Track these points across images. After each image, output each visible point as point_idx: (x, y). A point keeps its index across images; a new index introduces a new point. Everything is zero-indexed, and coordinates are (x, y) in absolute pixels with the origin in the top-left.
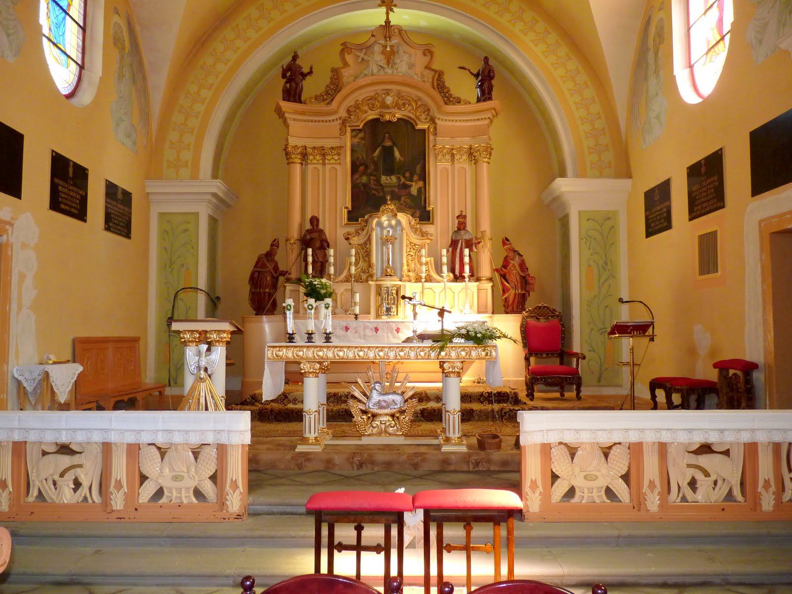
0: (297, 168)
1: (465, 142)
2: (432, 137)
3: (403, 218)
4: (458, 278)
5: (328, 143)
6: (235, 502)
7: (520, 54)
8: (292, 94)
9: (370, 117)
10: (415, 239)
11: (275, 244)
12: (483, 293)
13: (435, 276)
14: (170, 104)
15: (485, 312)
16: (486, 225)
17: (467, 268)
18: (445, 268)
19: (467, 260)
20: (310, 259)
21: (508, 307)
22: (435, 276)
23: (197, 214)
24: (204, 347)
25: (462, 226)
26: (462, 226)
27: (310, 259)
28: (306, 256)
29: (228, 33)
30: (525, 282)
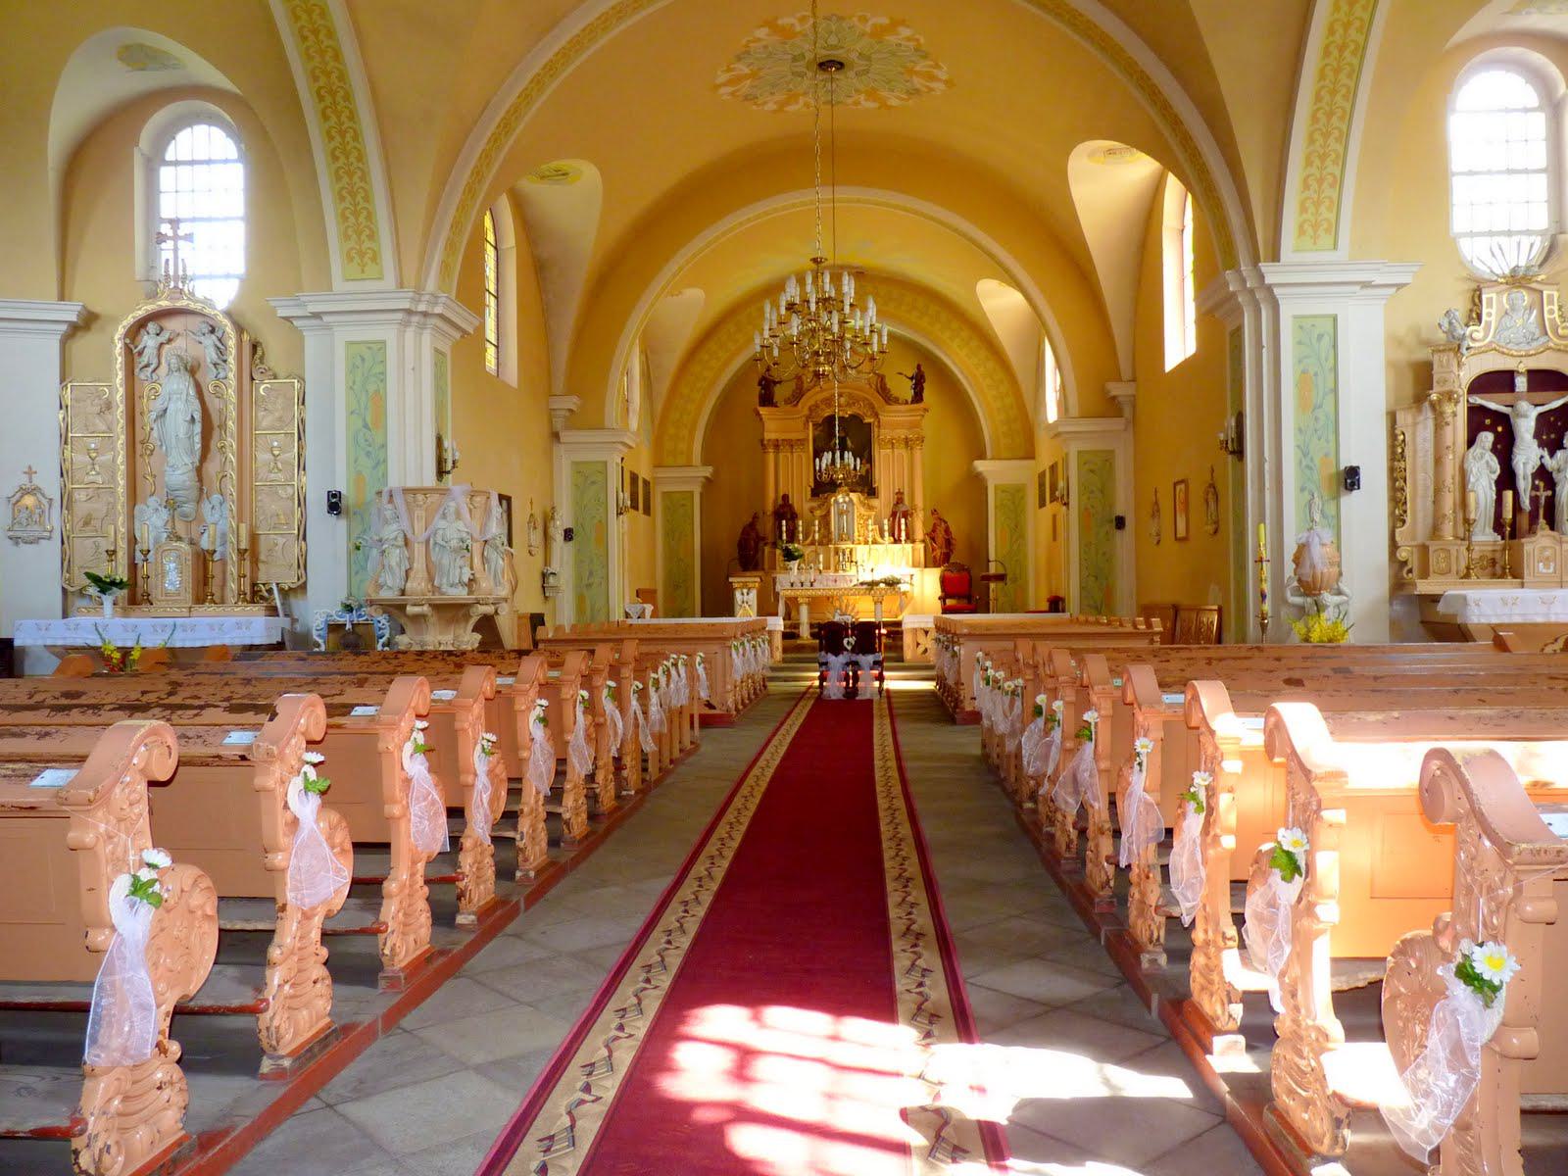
0: (771, 457)
1: (902, 433)
2: (876, 429)
3: (854, 496)
4: (897, 541)
5: (793, 436)
6: (779, 655)
7: (946, 355)
8: (767, 400)
9: (826, 415)
10: (863, 511)
11: (755, 517)
12: (916, 553)
13: (879, 539)
14: (667, 408)
15: (919, 566)
16: (919, 502)
17: (903, 534)
18: (886, 534)
19: (903, 527)
20: (784, 528)
21: (930, 562)
22: (879, 539)
23: (692, 493)
24: (745, 591)
25: (899, 501)
26: (899, 501)
27: (784, 528)
28: (781, 526)
29: (712, 345)
30: (949, 543)
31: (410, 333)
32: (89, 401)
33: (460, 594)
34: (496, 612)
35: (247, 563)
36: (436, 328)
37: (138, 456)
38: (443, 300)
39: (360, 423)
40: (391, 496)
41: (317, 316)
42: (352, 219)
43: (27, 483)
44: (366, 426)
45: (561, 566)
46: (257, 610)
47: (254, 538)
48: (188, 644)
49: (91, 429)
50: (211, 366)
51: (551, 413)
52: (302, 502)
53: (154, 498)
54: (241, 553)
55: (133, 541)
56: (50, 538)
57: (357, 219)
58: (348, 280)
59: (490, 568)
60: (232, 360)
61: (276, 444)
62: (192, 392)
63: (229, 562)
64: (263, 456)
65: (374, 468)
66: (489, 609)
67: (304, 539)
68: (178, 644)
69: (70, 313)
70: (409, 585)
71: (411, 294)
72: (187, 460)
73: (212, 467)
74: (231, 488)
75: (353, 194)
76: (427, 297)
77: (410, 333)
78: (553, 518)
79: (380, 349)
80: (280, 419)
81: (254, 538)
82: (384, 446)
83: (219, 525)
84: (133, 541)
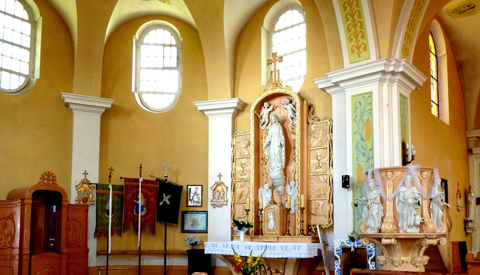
31: (385, 86)
32: (242, 142)
33: (414, 232)
34: (439, 243)
35: (305, 215)
36: (400, 81)
37: (260, 165)
38: (403, 63)
39: (359, 138)
40: (373, 174)
41: (336, 84)
42: (353, 30)
43: (218, 180)
44: (362, 139)
45: (475, 217)
46: (308, 239)
47: (308, 202)
48: (272, 256)
49: (243, 155)
50: (290, 119)
51: (467, 139)
52: (331, 183)
53: (266, 185)
54: (302, 209)
55: (257, 204)
56: (226, 205)
57: (355, 29)
58: (352, 63)
59: (434, 217)
60: (298, 113)
61: (319, 154)
62: (281, 132)
63: (297, 214)
64: (313, 161)
65: (367, 161)
66: (434, 242)
67: (332, 202)
68: (268, 256)
69: (234, 103)
70: (383, 226)
71: (384, 62)
72: (279, 165)
73: (291, 168)
74: (298, 177)
75: (353, 16)
76: (394, 62)
77: (385, 86)
78: (470, 192)
79: (369, 96)
80: (321, 141)
81: (308, 202)
82: (372, 149)
83: (294, 197)
84: (257, 204)
